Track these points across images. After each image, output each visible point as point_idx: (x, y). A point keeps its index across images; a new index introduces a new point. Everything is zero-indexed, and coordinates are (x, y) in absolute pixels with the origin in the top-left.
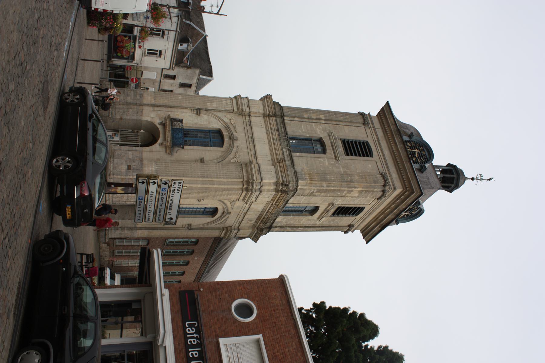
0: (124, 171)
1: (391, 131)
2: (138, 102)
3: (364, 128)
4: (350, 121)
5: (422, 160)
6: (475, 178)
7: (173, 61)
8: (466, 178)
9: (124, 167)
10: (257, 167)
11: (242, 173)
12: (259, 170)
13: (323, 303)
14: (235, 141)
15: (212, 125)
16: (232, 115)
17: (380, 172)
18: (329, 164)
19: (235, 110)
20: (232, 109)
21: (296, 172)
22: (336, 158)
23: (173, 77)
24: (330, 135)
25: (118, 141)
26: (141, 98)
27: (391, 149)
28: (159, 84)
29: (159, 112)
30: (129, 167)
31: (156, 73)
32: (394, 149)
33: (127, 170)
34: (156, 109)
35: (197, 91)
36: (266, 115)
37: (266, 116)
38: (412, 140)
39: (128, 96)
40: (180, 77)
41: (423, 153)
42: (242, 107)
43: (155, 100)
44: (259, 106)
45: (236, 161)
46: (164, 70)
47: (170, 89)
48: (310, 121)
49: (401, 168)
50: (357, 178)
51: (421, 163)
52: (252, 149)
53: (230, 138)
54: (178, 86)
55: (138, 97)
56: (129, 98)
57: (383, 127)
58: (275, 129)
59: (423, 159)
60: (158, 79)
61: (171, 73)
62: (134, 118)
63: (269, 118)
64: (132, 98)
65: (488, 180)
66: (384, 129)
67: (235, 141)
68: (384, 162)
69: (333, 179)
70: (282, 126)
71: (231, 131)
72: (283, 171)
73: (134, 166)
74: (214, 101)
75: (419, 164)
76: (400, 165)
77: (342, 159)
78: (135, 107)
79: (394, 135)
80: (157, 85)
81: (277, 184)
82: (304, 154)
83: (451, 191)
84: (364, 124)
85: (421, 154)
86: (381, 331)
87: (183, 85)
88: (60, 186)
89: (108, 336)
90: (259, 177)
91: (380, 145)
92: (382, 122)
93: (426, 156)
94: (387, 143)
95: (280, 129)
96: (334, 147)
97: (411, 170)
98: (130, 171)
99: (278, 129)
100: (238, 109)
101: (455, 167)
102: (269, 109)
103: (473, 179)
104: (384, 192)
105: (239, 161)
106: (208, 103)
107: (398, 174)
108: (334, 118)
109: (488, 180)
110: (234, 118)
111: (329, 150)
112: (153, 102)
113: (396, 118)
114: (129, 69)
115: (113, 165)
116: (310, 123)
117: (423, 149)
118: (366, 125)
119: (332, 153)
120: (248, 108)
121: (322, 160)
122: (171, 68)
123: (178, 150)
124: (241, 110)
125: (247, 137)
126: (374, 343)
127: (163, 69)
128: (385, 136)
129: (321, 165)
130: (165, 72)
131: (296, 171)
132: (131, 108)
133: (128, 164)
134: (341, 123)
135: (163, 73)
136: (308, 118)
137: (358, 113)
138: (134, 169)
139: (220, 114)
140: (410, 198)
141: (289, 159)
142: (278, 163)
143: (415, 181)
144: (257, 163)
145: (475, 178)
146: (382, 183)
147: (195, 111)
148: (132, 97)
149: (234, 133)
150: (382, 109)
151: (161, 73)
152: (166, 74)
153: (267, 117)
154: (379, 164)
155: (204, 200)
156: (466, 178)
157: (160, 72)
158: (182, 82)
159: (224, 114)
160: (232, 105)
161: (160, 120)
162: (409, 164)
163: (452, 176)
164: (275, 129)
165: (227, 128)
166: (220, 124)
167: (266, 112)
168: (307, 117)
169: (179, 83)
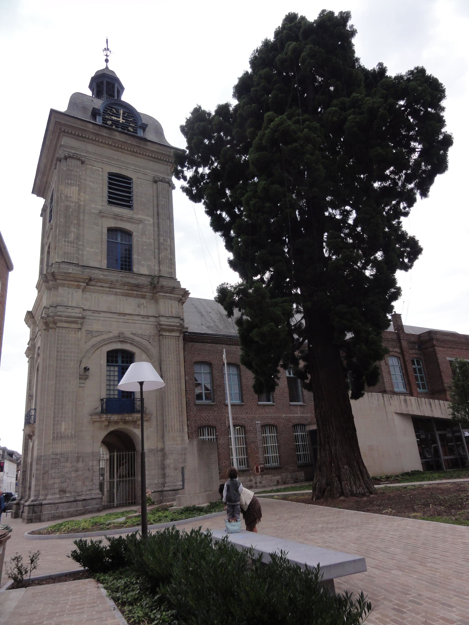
6: (106, 57)
8: (107, 68)
13: (357, 33)
27: (145, 157)
65: (107, 40)
66: (168, 164)
83: (123, 89)
86: (454, 141)
88: (237, 213)
89: (221, 480)
101: (93, 79)
103: (107, 61)
104: (66, 158)
109: (107, 40)
126: (231, 109)
144: (49, 308)
145: (106, 57)
149: (111, 335)
155: (86, 369)
156: (107, 68)
163: (105, 84)
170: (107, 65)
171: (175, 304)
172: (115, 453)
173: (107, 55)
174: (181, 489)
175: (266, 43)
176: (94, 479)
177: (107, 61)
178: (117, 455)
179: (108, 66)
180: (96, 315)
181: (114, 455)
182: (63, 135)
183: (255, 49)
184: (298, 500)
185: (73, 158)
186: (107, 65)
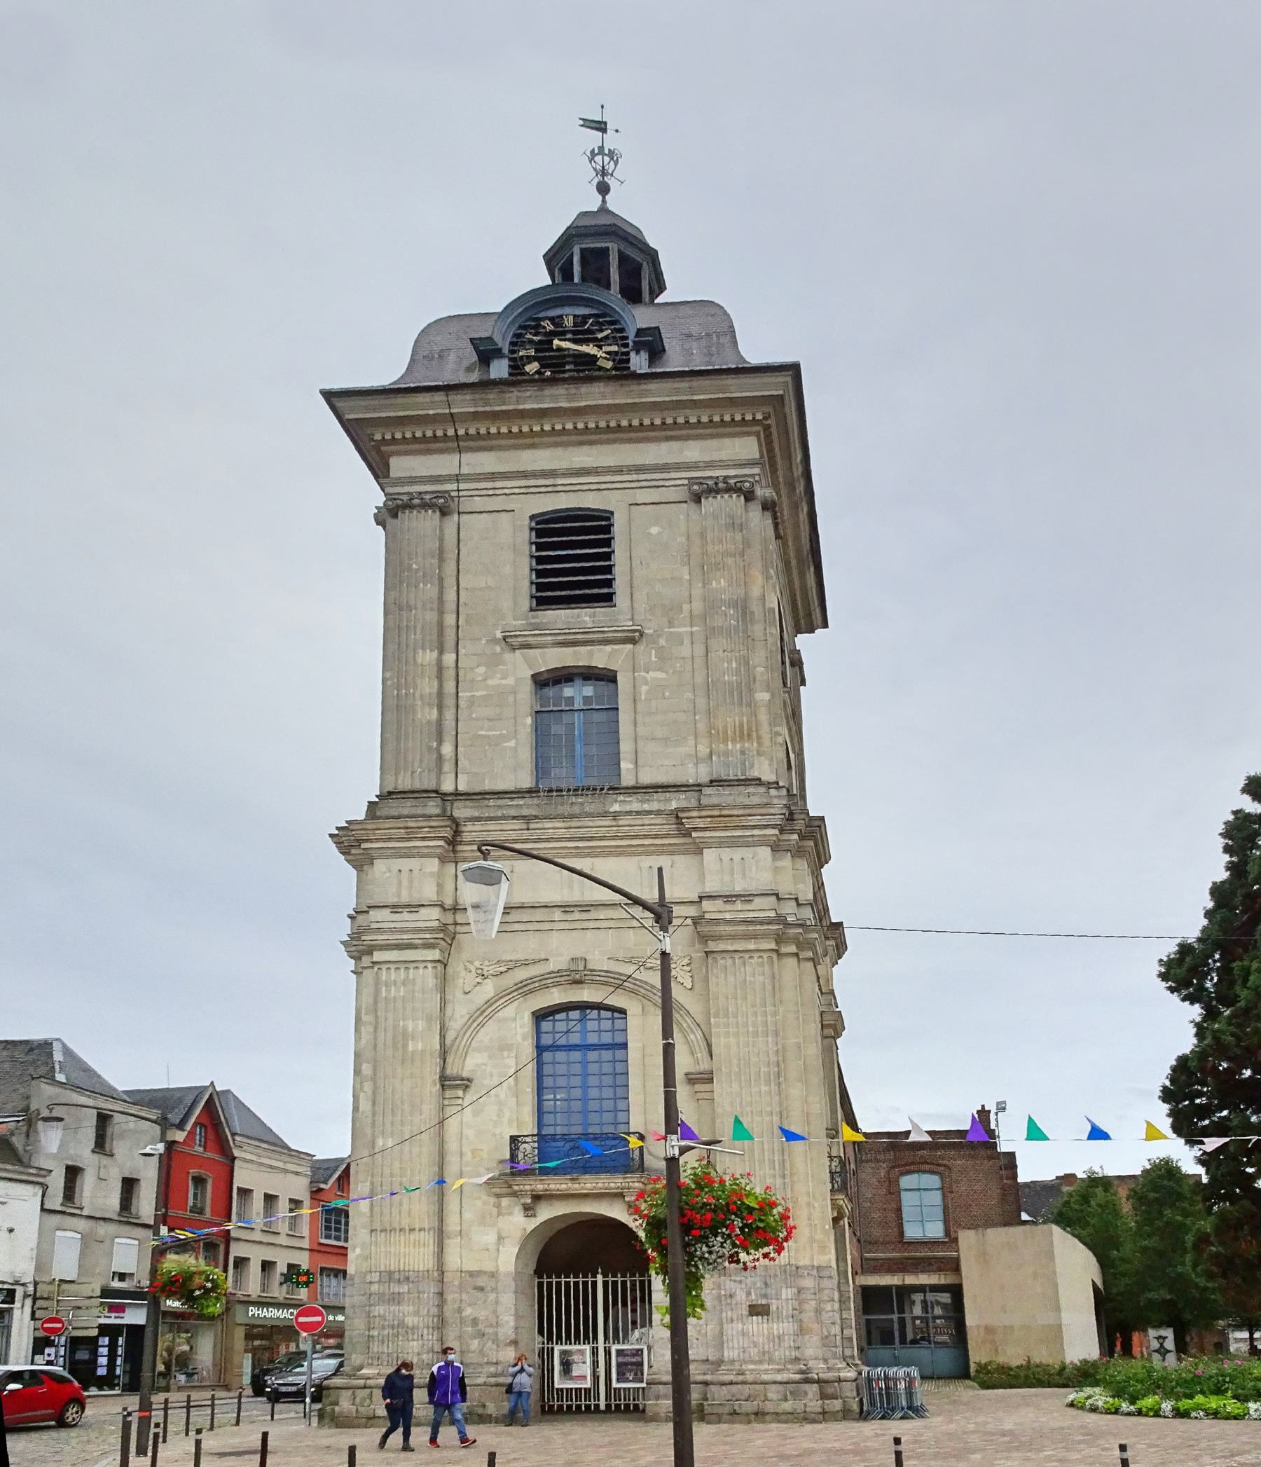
0: (778, 1328)
1: (476, 416)
2: (433, 1288)
3: (464, 518)
4: (435, 561)
5: (606, 337)
7: (14, 1172)
8: (603, 209)
9: (756, 1325)
10: (719, 904)
11: (747, 956)
12: (729, 898)
14: (590, 966)
15: (519, 1038)
16: (456, 966)
17: (686, 502)
18: (660, 669)
19: (435, 954)
20: (429, 965)
21: (712, 783)
22: (633, 641)
23: (73, 1173)
24: (510, 642)
25: (595, 1352)
26: (407, 1279)
28: (101, 1223)
29: (467, 1215)
30: (758, 1310)
31: (58, 1233)
32: (547, 428)
33: (773, 1315)
34: (452, 1223)
35: (118, 1094)
36: (447, 851)
37: (454, 851)
38: (506, 351)
39: (402, 1324)
40: (72, 1152)
41: (569, 322)
42: (427, 930)
43: (411, 1230)
44: (405, 874)
45: (688, 968)
46: (45, 1207)
47: (118, 1186)
48: (450, 702)
49: (675, 418)
50: (719, 583)
51: (626, 345)
52: (539, 915)
53: (580, 982)
54: (105, 1161)
55: (404, 1288)
56: (410, 1321)
57: (450, 444)
58: (524, 826)
59: (602, 331)
60: (82, 1224)
61: (57, 1181)
62: (508, 1299)
63: (461, 843)
64: (411, 1308)
67: (590, 966)
68: (635, 477)
69: (734, 665)
70: (491, 803)
71: (543, 977)
72: (734, 822)
73: (749, 1294)
74: (395, 1027)
75: (627, 354)
76: (647, 422)
77: (632, 619)
78: (449, 1297)
79: (504, 408)
80: (103, 1230)
81: (776, 848)
82: (625, 747)
84: (444, 512)
85: (574, 333)
87: (101, 1144)
90: (759, 902)
91: (553, 474)
92: (424, 439)
93: (590, 316)
94: (533, 446)
95: (525, 812)
96: (579, 637)
97: (683, 384)
98: (773, 1308)
99: (527, 819)
100: (431, 946)
102: (423, 839)
103: (603, 189)
105: (686, 961)
106: (410, 1048)
107: (688, 438)
108: (431, 616)
110: (471, 962)
111: (599, 658)
112: (429, 1239)
113: (393, 383)
114: (59, 1325)
115: (752, 1362)
116: (462, 703)
117: (552, 319)
118: (453, 506)
119: (608, 648)
120: (423, 911)
121: (644, 688)
122: (41, 1180)
123: (651, 1154)
124: (441, 936)
125: (562, 925)
127: (43, 1209)
128: (500, 448)
129: (667, 694)
130: (56, 1202)
131: (711, 781)
132: (460, 1310)
133: (745, 1312)
134: (450, 595)
135: (59, 1208)
136: (440, 707)
137: (380, 521)
138: (765, 1296)
139: (459, 1012)
140: (374, 410)
141: (661, 796)
142: (694, 834)
143: (730, 381)
146: (737, 501)
147: (448, 1093)
148: (407, 1308)
149: (552, 966)
150: (353, 429)
151: (59, 1217)
152: (60, 1199)
153: (459, 848)
154: (642, 496)
156: (603, 209)
157: (56, 1219)
158: (92, 1144)
159: (455, 995)
160: (412, 966)
161: (510, 1214)
162: (653, 386)
164: (524, 826)
165: (525, 989)
166: (510, 1011)
167: (439, 851)
168: (435, 710)
169: (96, 1157)
170: (604, 201)
171: (1167, 1340)
172: (600, 1278)
173: (604, 172)
174: (42, 1204)
175: (1217, 891)
176: (495, 1361)
177: (603, 189)
178: (605, 1284)
179: (600, 198)
180: (577, 916)
181: (594, 1284)
182: (758, 435)
183: (1175, 998)
184: (347, 1224)
185: (718, 491)
186: (604, 201)
